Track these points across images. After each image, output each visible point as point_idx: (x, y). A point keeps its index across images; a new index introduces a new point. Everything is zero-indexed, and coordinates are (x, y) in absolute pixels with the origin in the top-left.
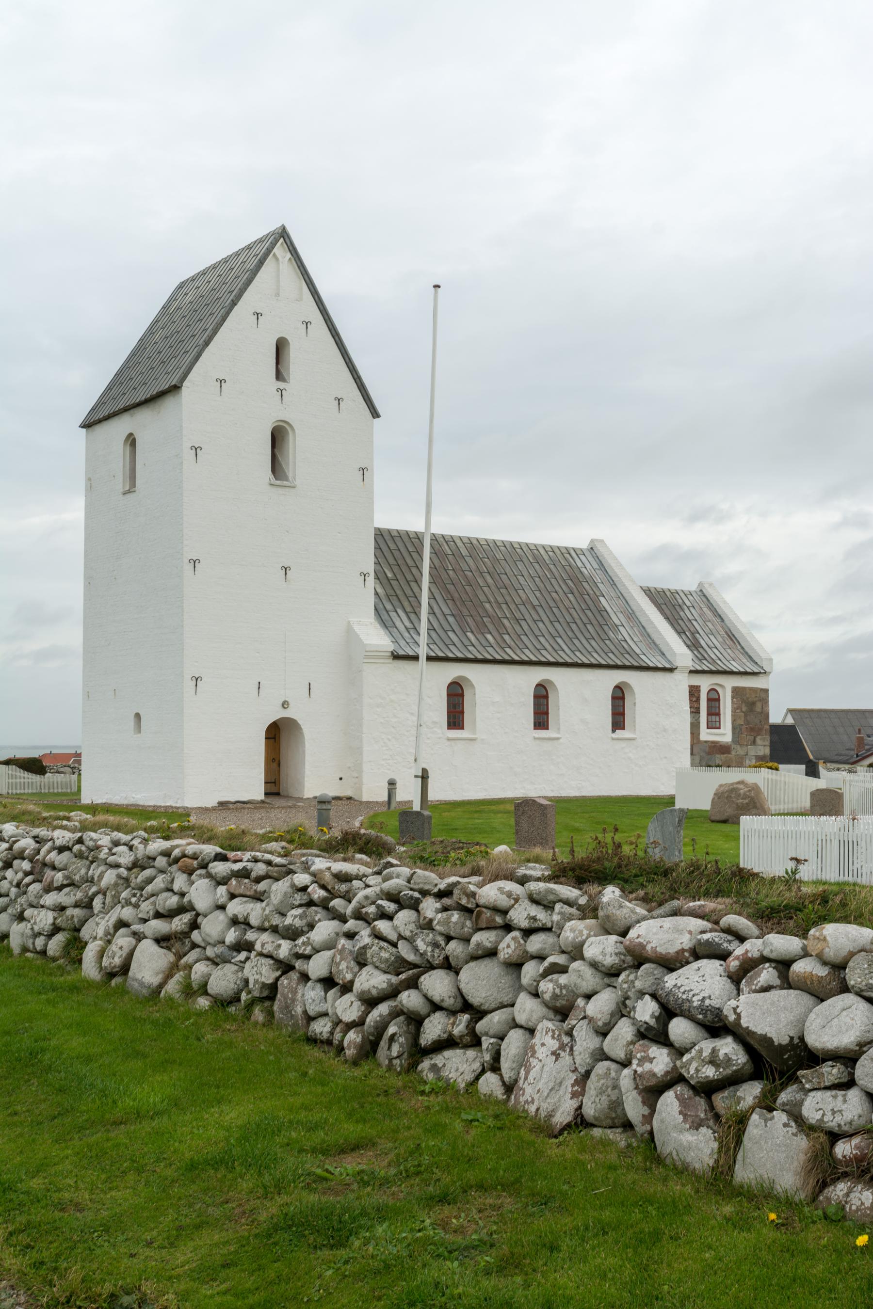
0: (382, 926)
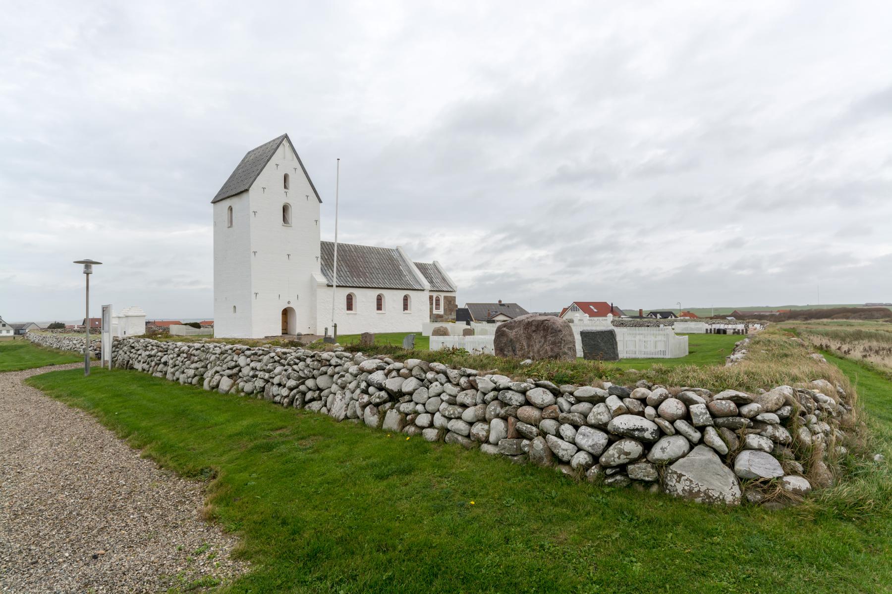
0: (295, 367)
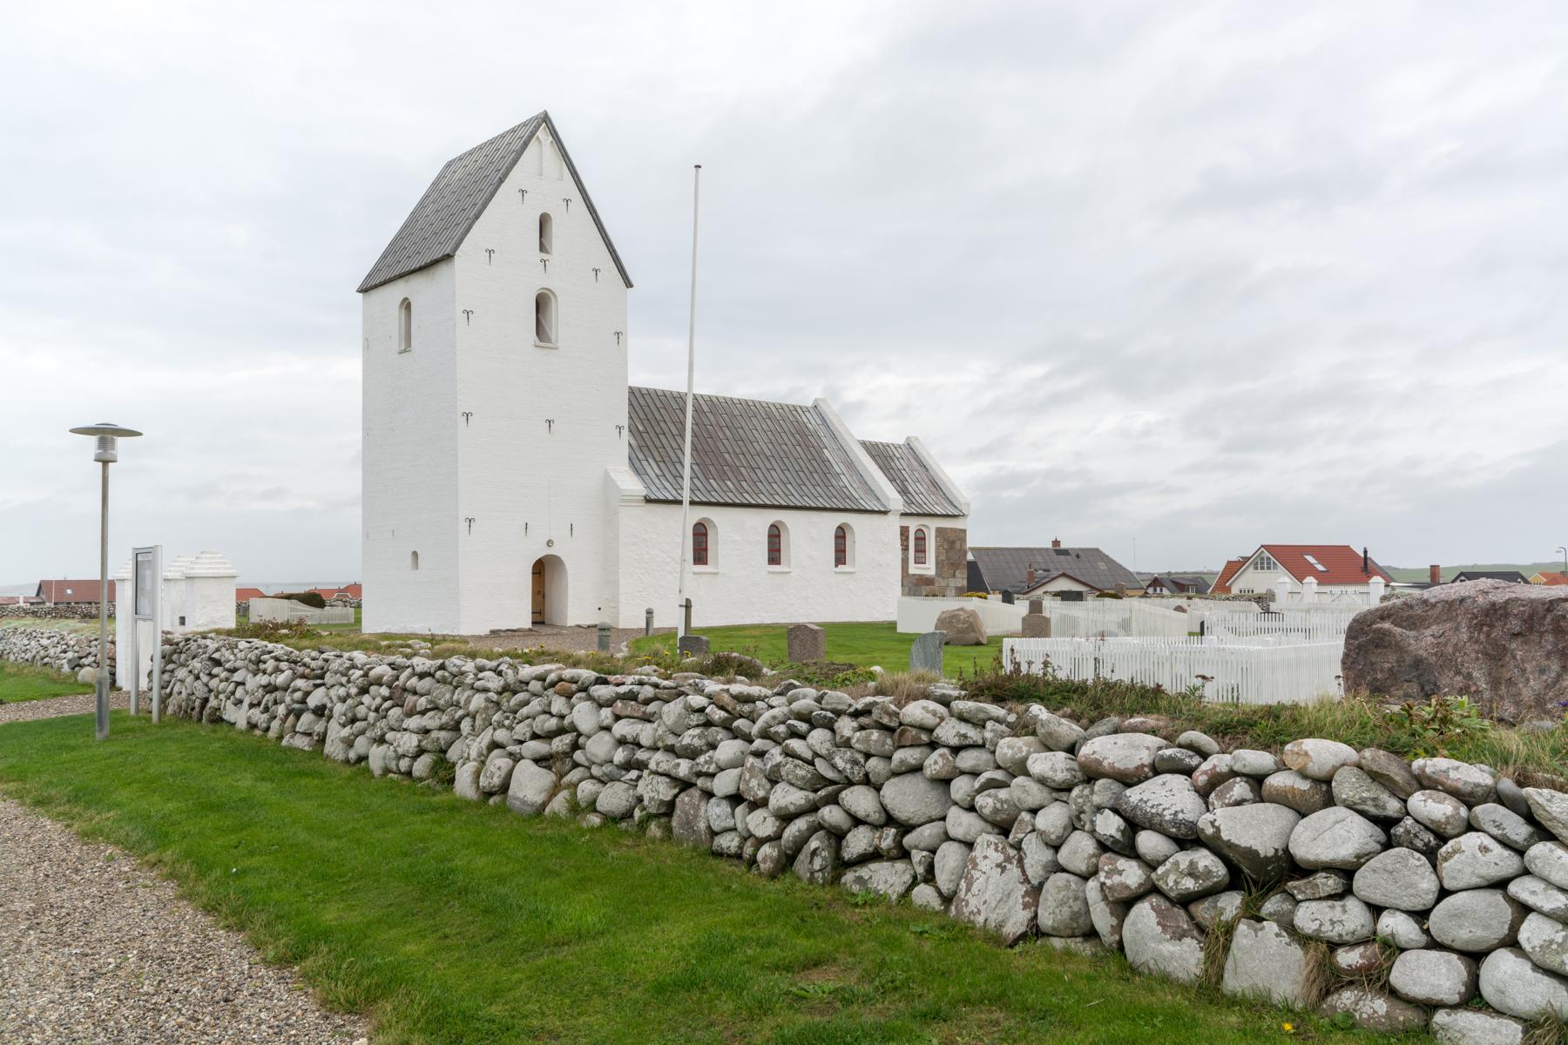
0: (795, 744)
